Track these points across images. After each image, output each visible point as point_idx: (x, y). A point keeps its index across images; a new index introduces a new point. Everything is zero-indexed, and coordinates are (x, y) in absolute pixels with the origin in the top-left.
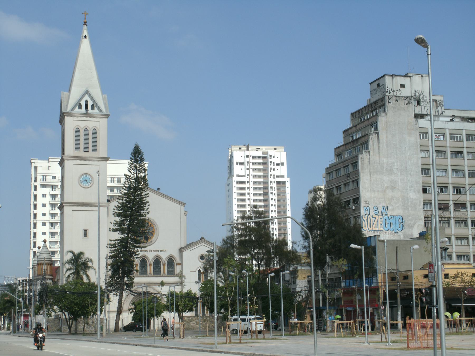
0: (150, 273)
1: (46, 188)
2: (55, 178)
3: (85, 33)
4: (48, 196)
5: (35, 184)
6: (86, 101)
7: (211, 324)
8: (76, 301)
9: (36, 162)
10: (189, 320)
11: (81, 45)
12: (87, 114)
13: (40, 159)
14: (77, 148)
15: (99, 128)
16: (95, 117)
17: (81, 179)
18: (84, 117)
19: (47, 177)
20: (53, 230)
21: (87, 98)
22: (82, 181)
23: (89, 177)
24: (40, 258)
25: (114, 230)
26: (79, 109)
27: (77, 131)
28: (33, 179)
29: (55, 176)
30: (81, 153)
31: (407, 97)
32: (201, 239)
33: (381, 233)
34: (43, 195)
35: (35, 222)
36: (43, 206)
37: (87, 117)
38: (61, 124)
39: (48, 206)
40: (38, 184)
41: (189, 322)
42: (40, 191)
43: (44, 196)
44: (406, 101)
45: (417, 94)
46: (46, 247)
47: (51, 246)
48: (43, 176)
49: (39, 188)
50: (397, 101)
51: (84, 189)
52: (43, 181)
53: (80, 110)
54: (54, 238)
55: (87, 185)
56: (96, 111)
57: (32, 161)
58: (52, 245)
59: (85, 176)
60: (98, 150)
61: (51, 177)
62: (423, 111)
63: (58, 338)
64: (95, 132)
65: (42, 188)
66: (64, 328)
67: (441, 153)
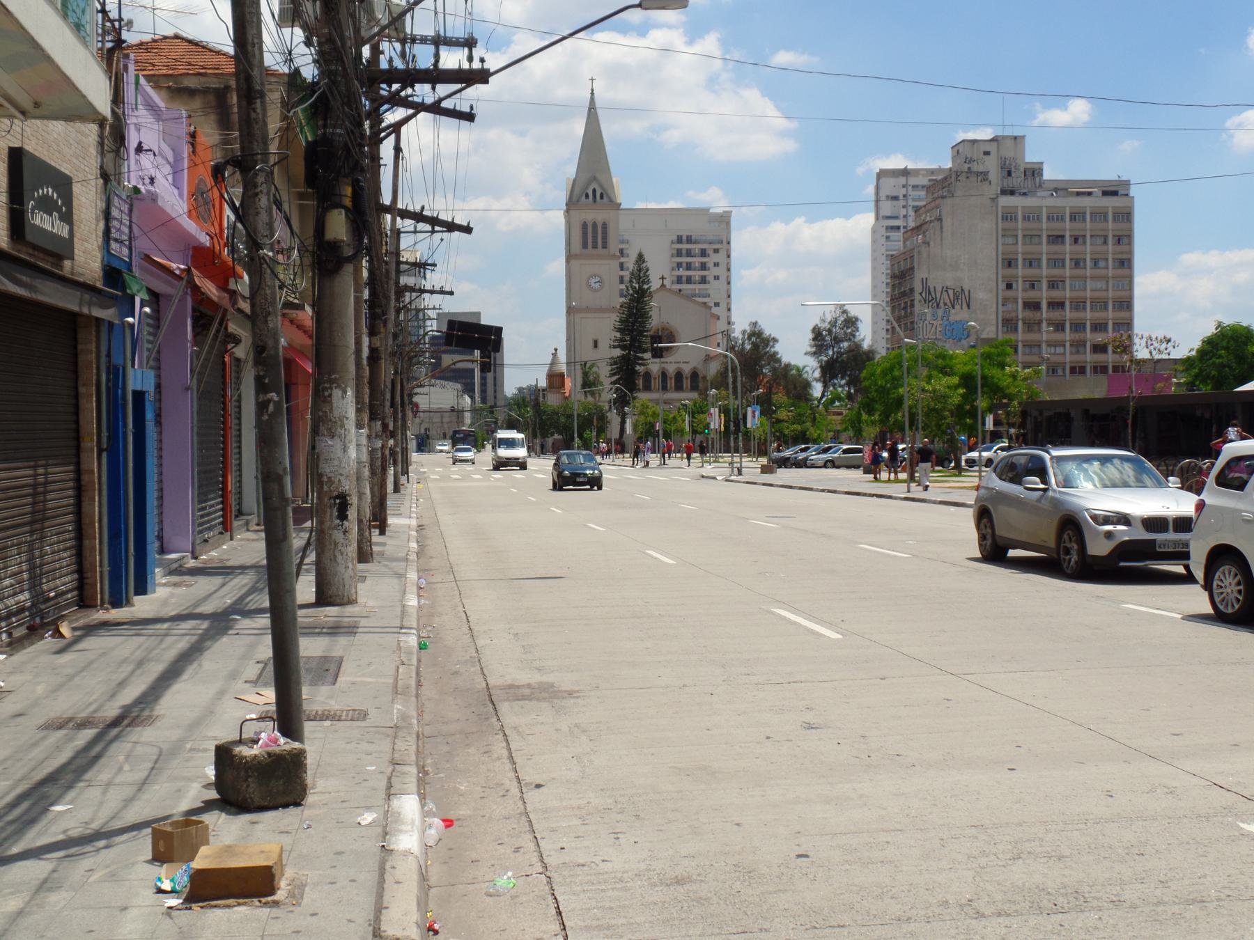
0: (671, 388)
25: (615, 347)
31: (982, 173)
33: (655, 366)
44: (980, 178)
45: (1007, 162)
50: (968, 177)
62: (1015, 183)
67: (1030, 237)
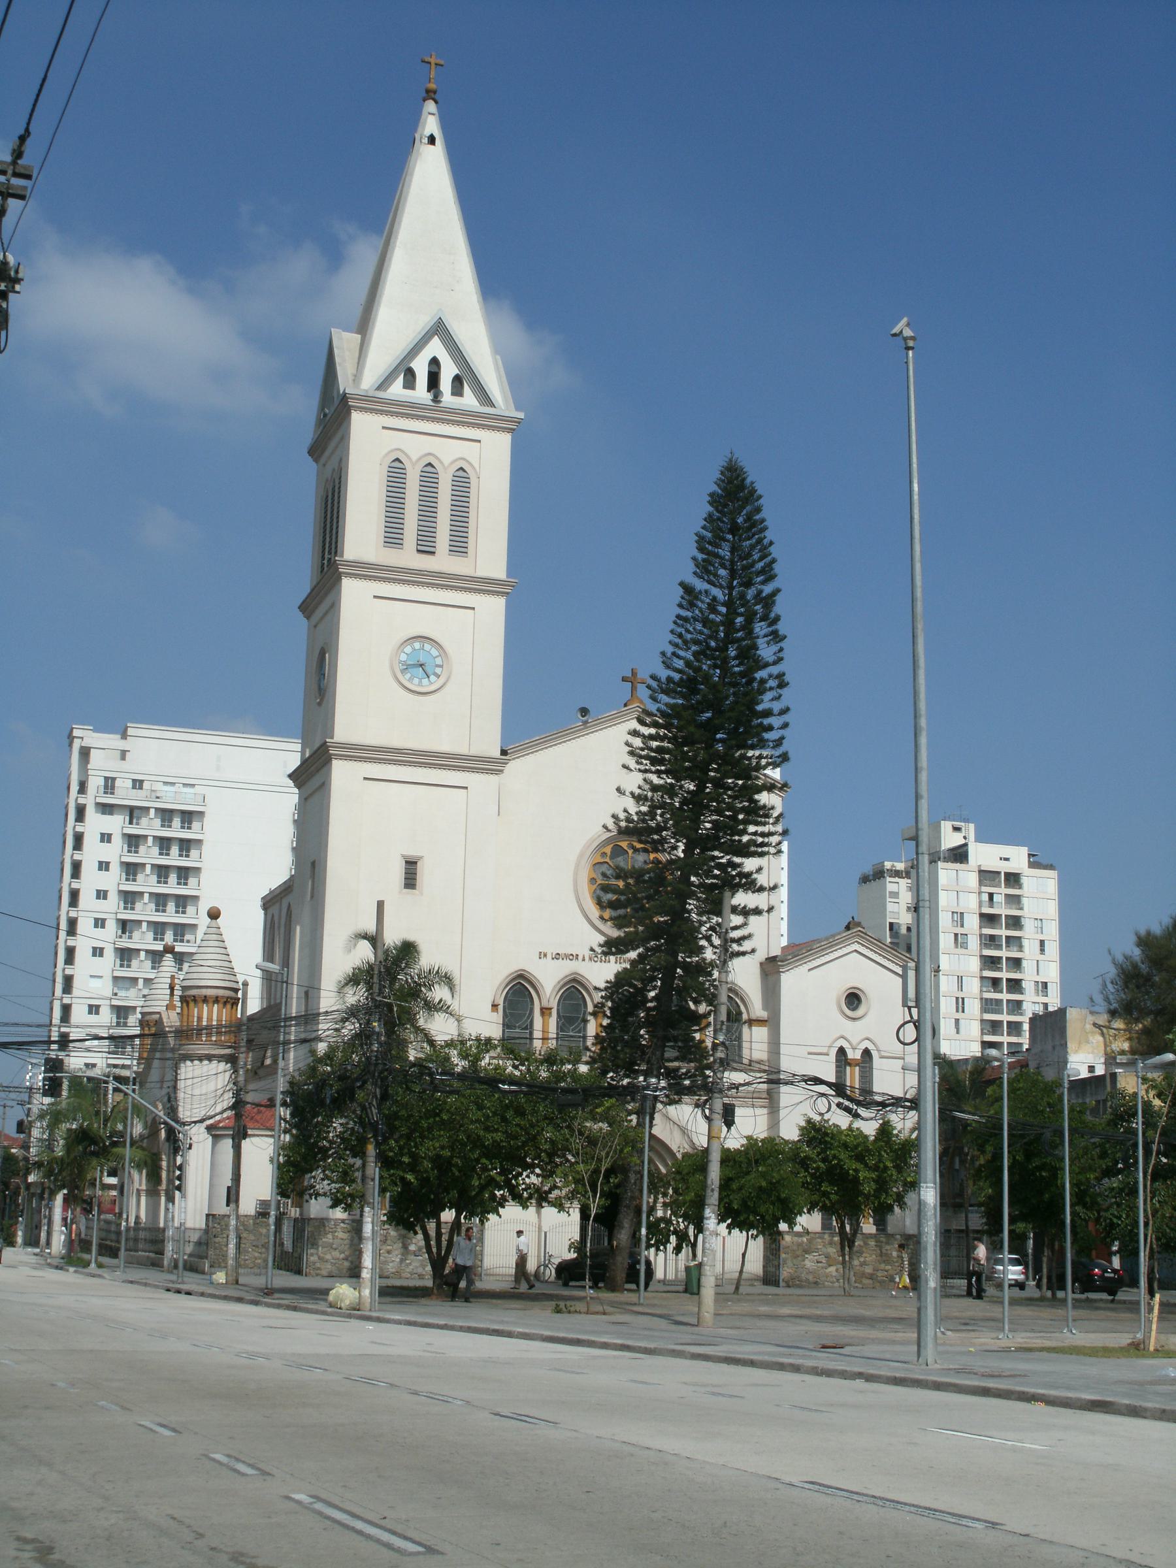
1: (111, 813)
2: (141, 788)
3: (431, 125)
4: (117, 840)
5: (81, 801)
6: (434, 362)
7: (883, 1266)
8: (489, 1138)
9: (85, 736)
10: (800, 1245)
11: (415, 165)
12: (434, 411)
13: (101, 728)
14: (393, 537)
15: (476, 466)
16: (458, 423)
17: (403, 657)
18: (423, 418)
19: (118, 783)
20: (125, 943)
21: (435, 348)
22: (407, 667)
23: (434, 652)
24: (195, 976)
26: (405, 387)
27: (396, 471)
28: (75, 787)
29: (141, 782)
30: (408, 557)
32: (848, 928)
34: (103, 835)
35: (73, 914)
36: (100, 869)
37: (434, 420)
38: (316, 460)
39: (115, 869)
40: (89, 801)
41: (799, 1253)
42: (95, 823)
43: (106, 838)
46: (218, 937)
47: (116, 991)
48: (106, 779)
49: (90, 812)
51: (411, 696)
52: (105, 793)
53: (409, 392)
54: (129, 966)
55: (425, 681)
56: (469, 400)
57: (76, 733)
58: (119, 988)
59: (417, 645)
60: (471, 550)
61: (130, 784)
63: (397, 1317)
64: (462, 480)
65: (99, 815)
66: (312, 1259)
